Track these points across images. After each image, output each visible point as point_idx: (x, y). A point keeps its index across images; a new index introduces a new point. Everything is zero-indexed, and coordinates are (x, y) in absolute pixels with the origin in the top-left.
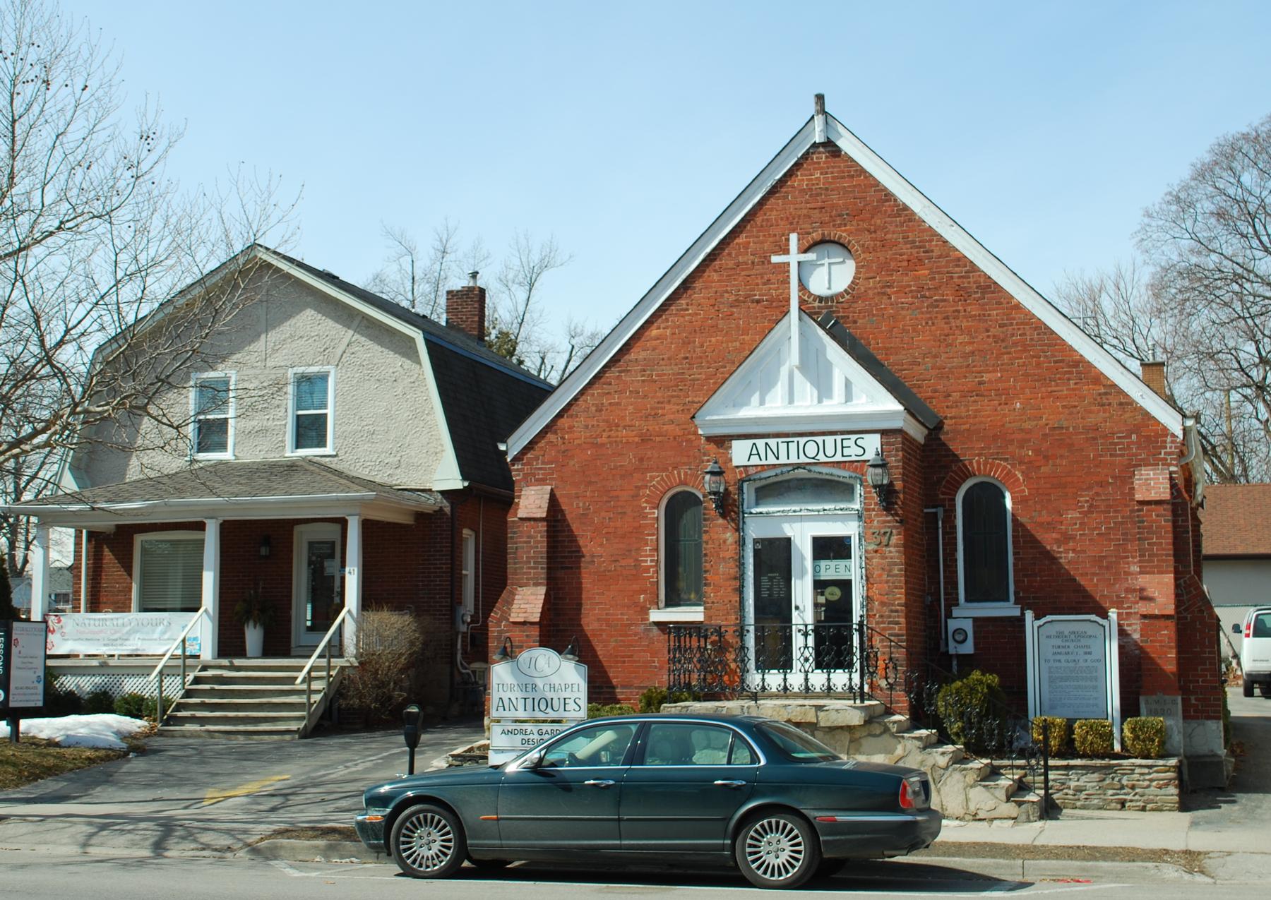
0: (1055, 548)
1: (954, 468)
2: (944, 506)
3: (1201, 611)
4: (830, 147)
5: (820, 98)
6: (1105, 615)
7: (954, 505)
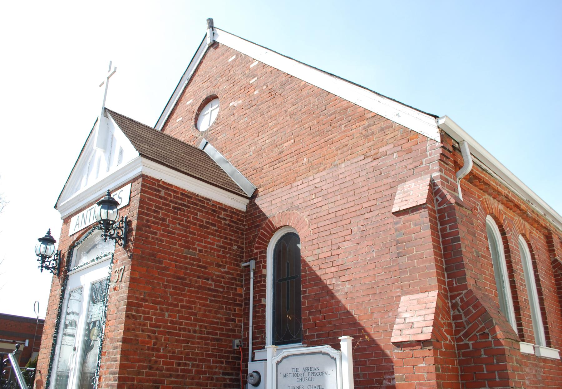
0: (334, 281)
1: (264, 225)
2: (255, 259)
3: (485, 336)
4: (215, 44)
5: (211, 21)
6: (337, 347)
7: (265, 257)
